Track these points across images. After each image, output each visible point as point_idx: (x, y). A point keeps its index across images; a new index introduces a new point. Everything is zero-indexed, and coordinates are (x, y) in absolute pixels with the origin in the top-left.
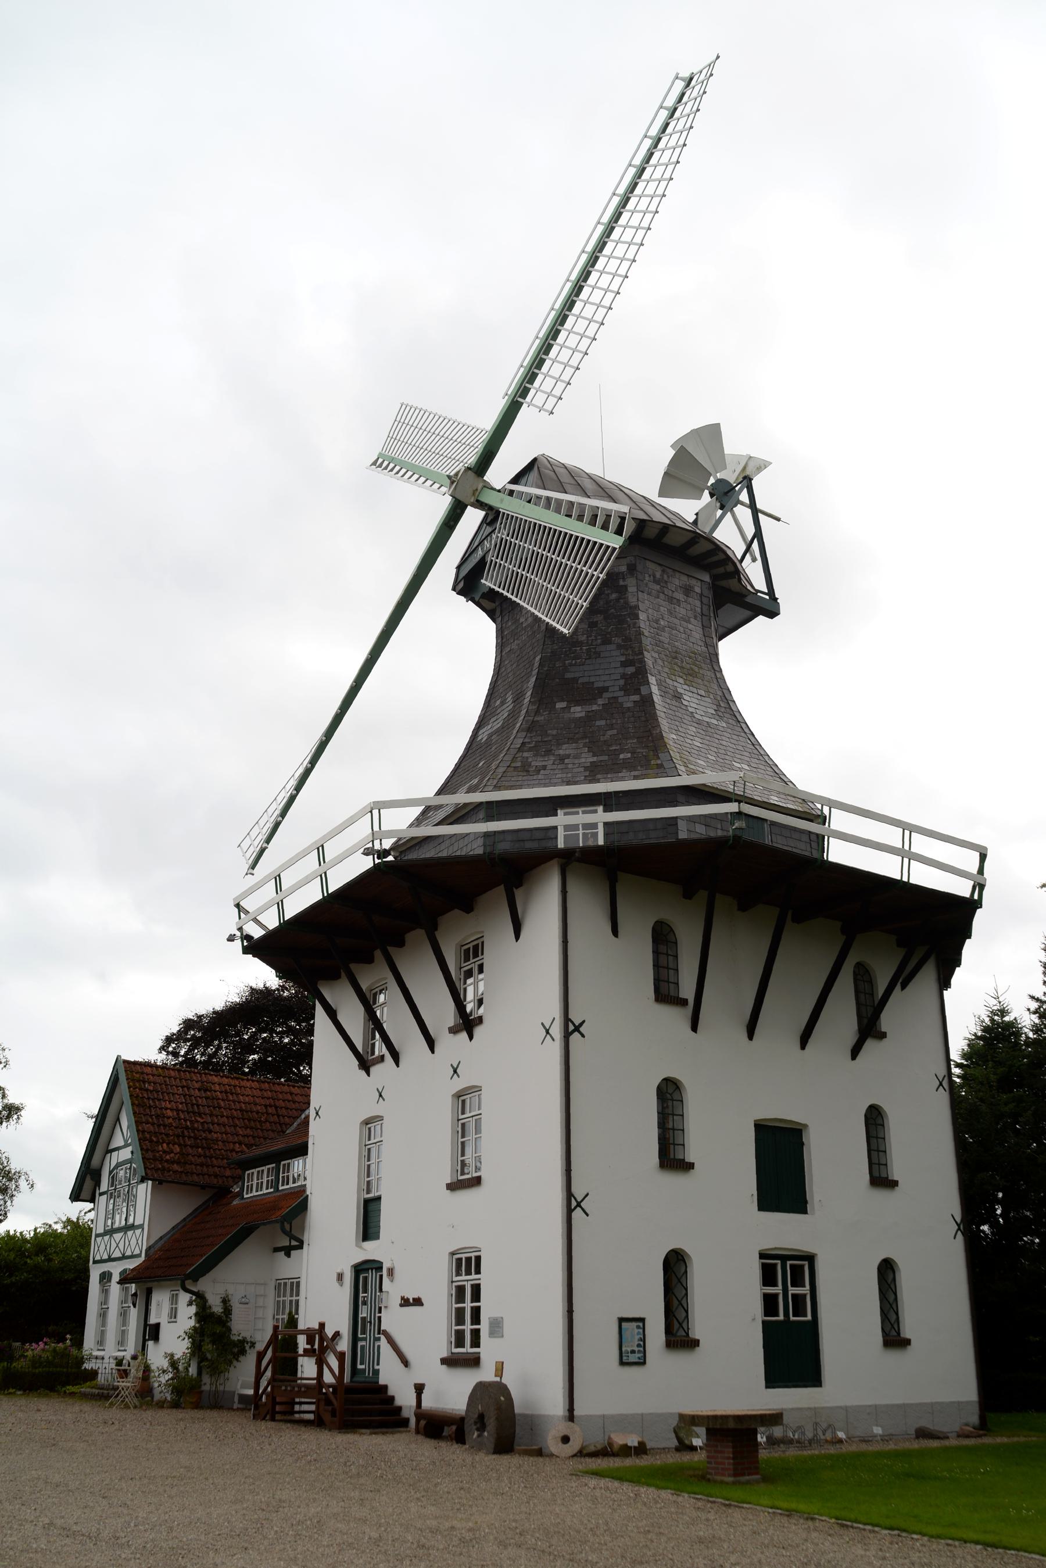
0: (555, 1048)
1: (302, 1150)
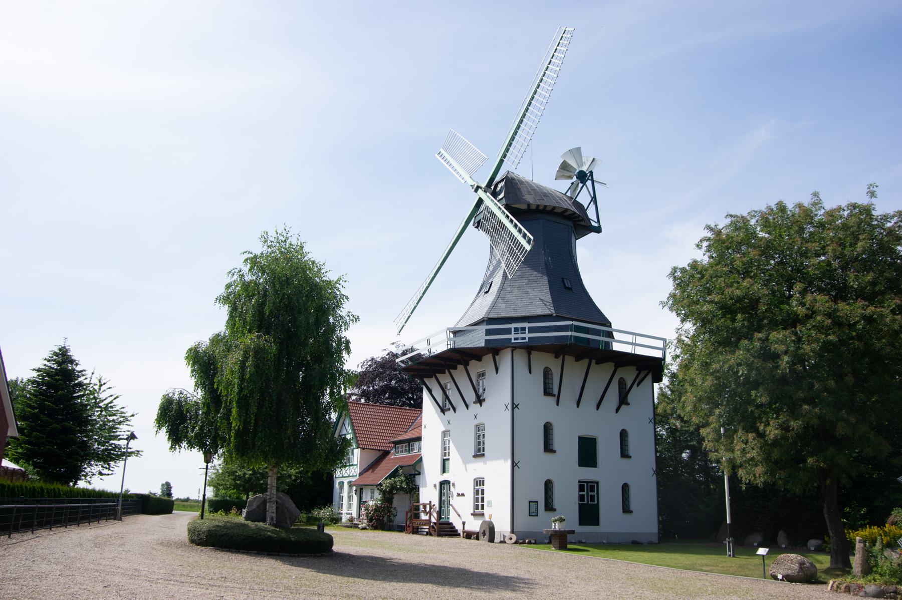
0: (509, 413)
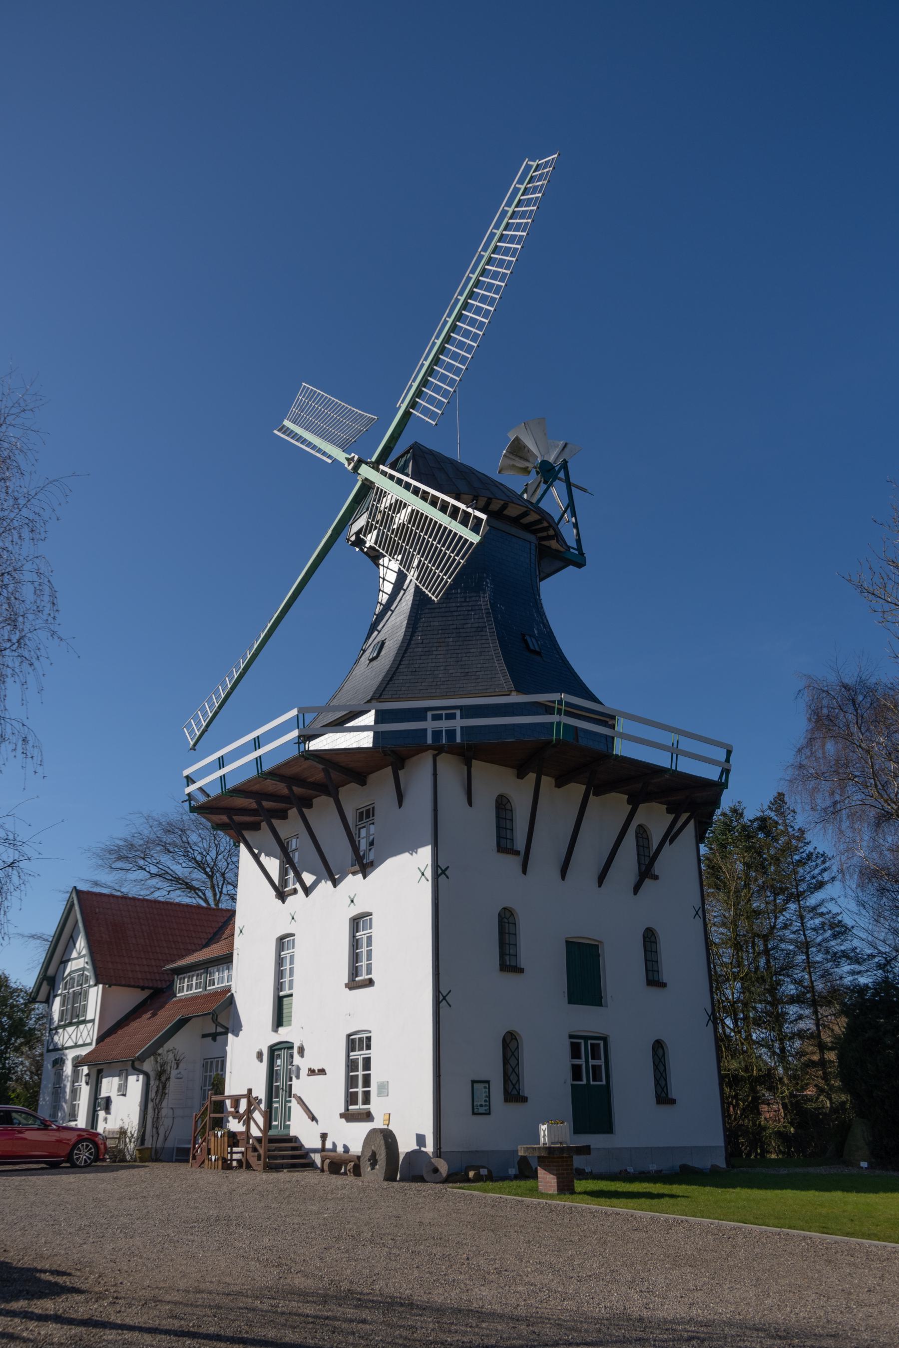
1: (226, 960)
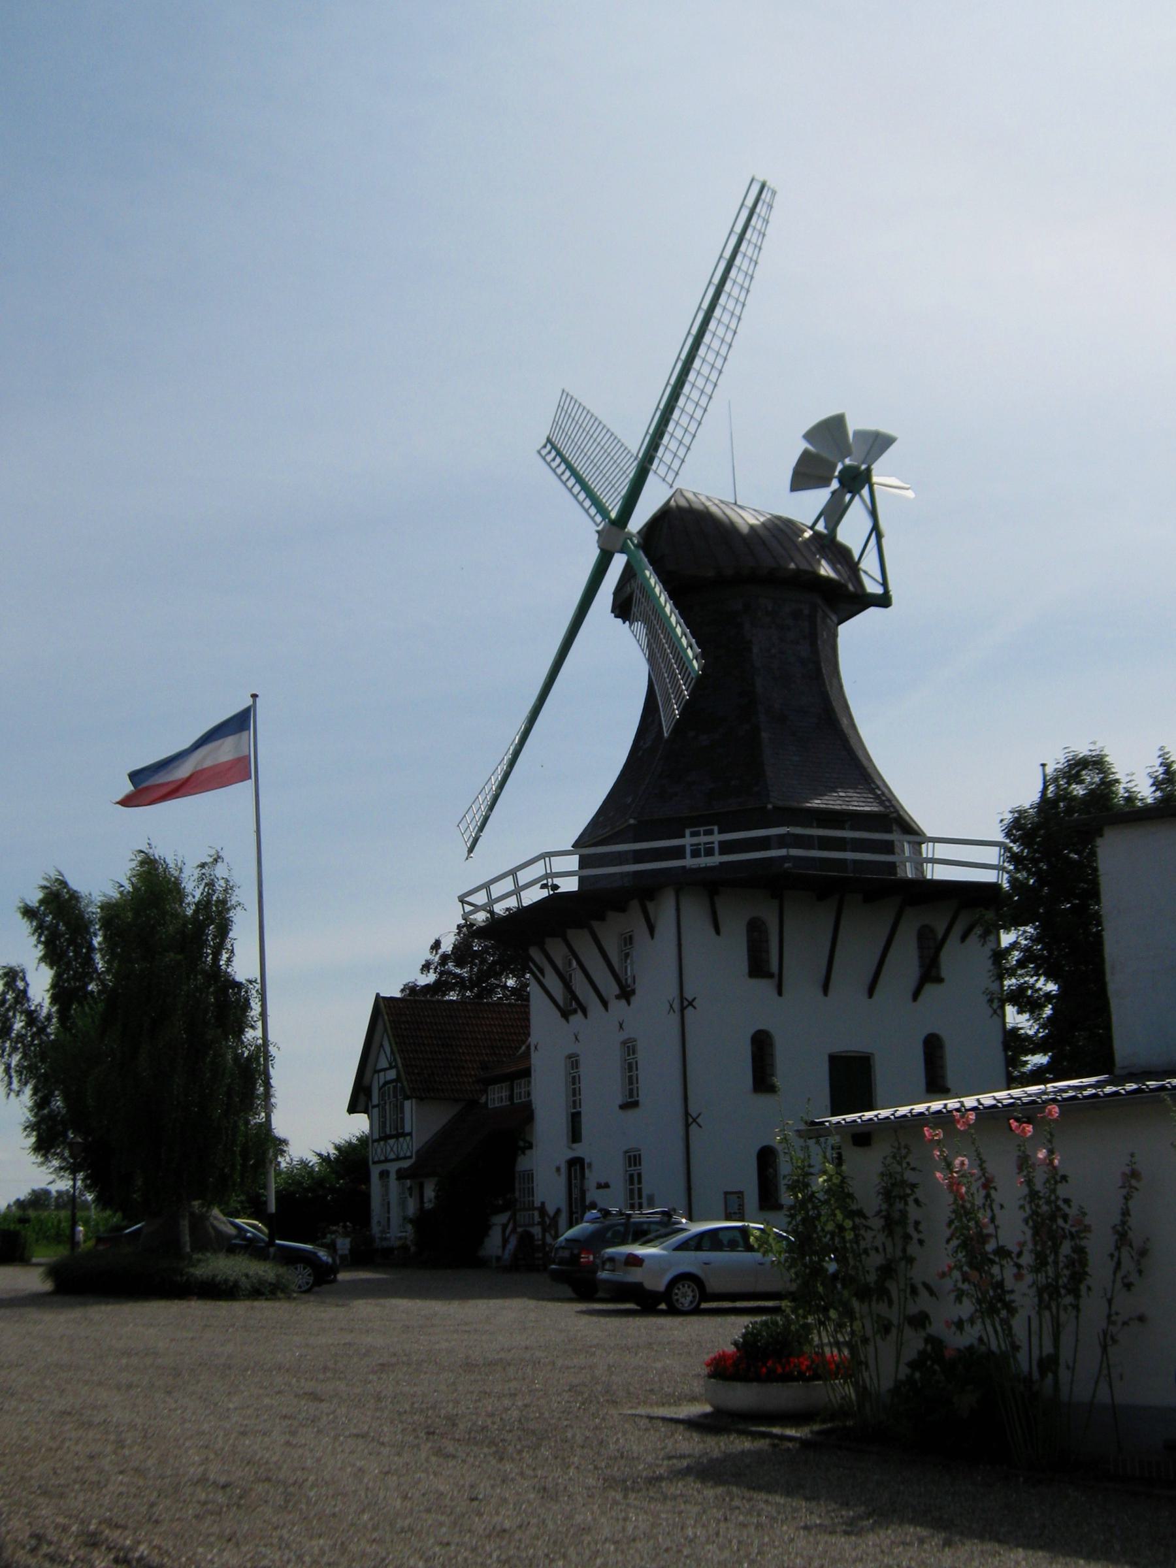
0: (675, 1018)
